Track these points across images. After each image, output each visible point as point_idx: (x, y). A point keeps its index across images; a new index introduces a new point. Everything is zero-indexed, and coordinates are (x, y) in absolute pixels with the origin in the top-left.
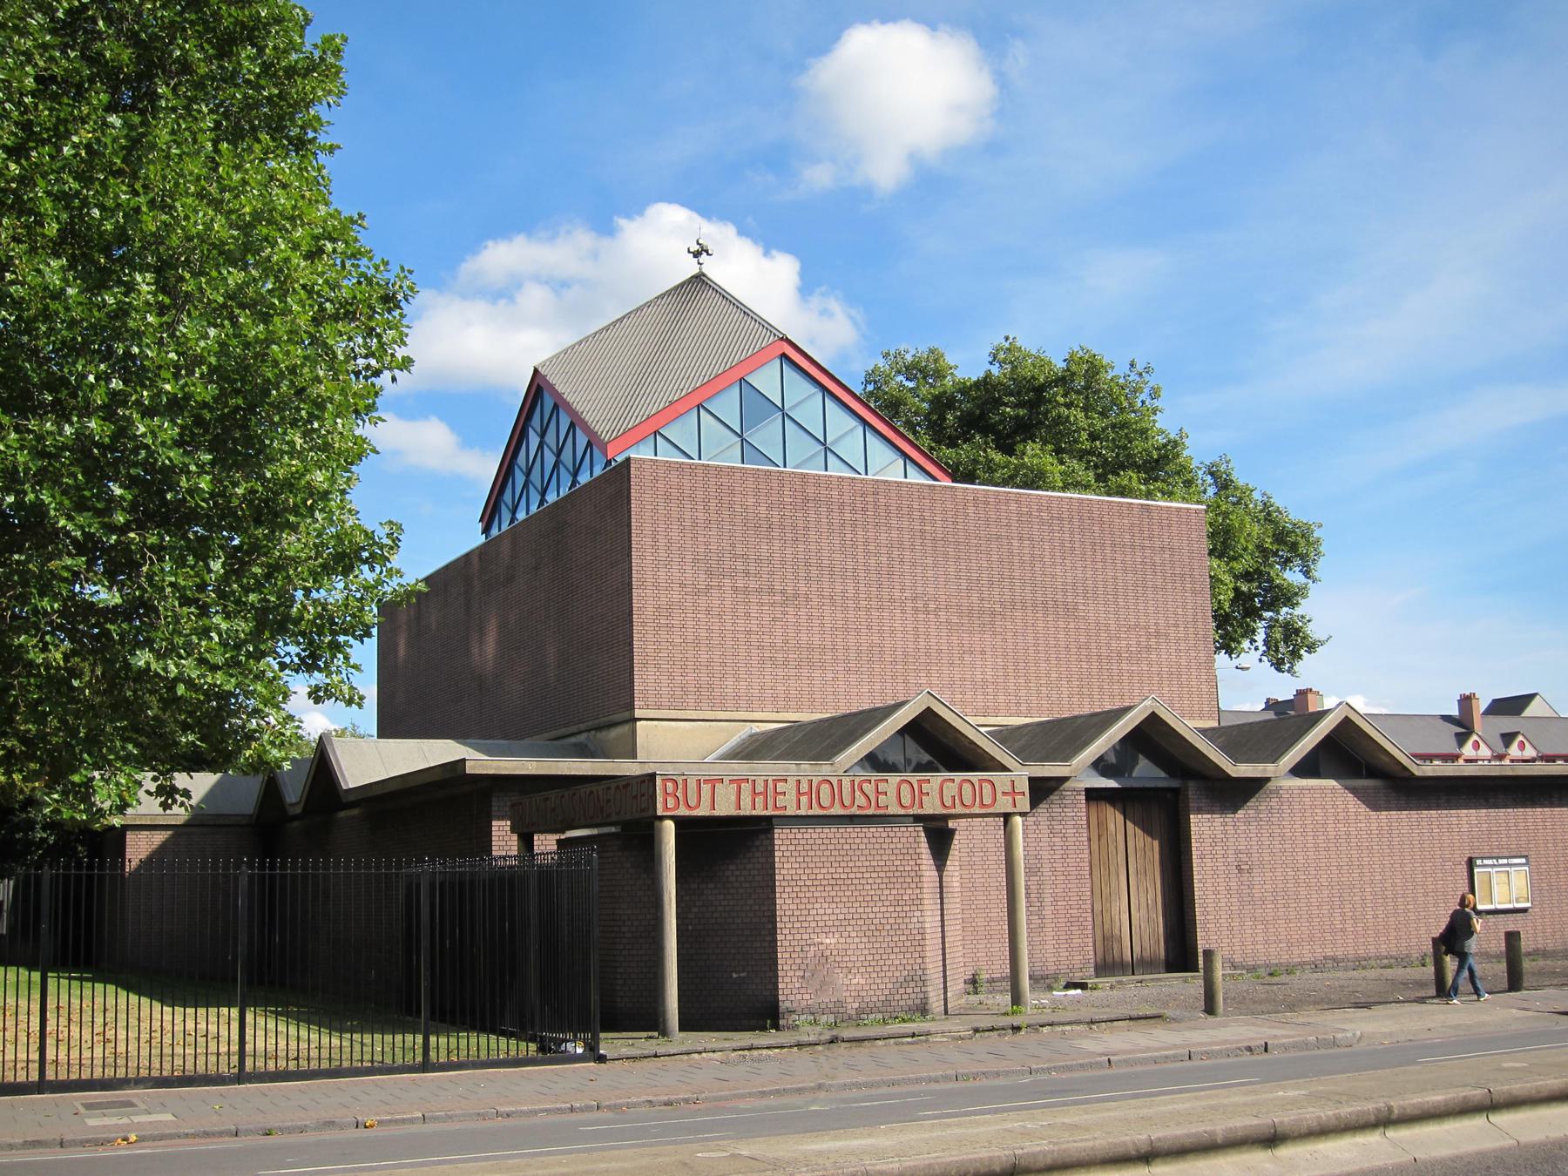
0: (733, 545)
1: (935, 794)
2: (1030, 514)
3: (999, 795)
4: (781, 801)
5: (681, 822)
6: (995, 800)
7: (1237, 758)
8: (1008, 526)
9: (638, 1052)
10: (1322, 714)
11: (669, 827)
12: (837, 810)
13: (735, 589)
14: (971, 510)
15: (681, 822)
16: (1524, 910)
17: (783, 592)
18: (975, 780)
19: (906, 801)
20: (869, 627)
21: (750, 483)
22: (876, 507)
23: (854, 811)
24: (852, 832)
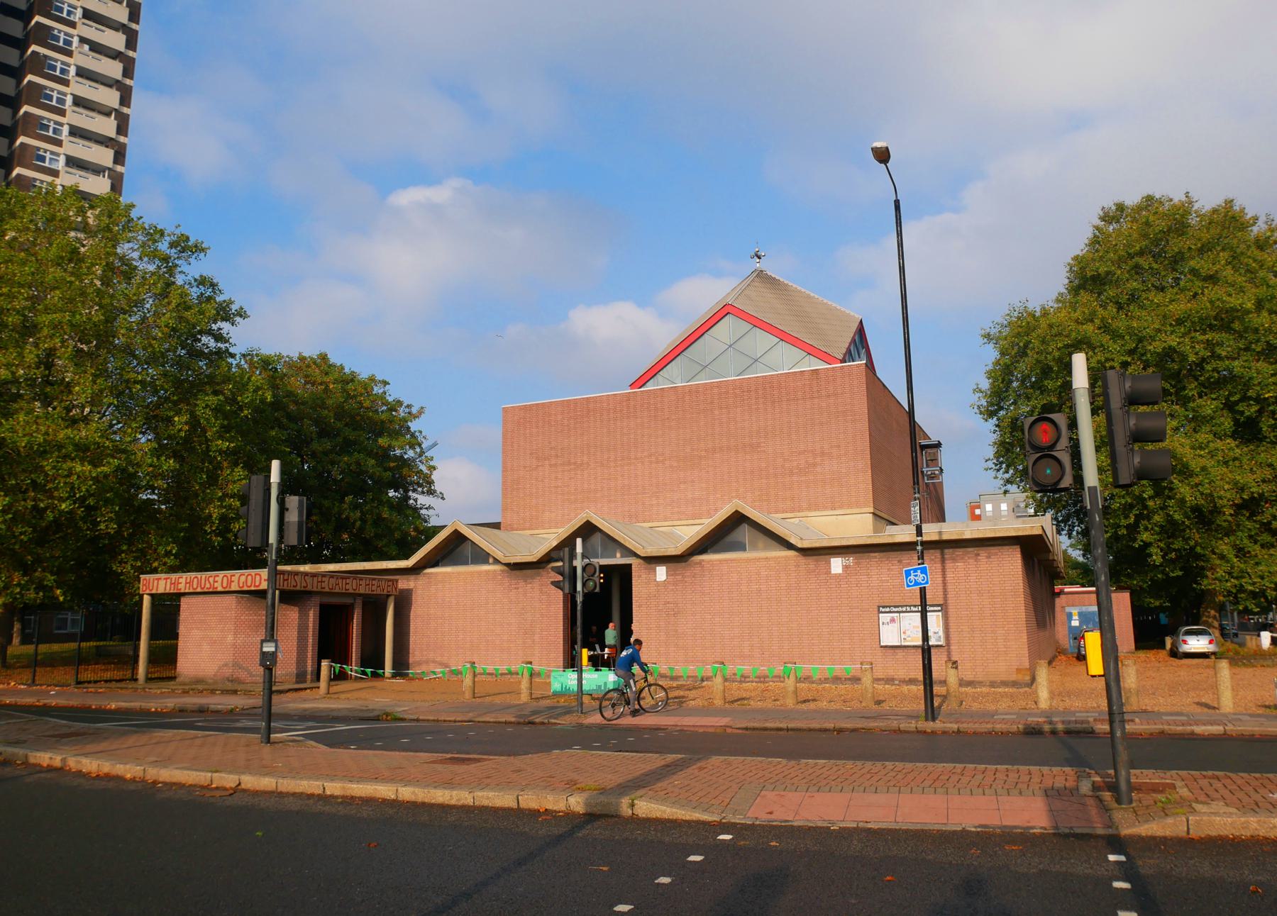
0: (550, 443)
1: (236, 581)
2: (727, 393)
3: (263, 581)
4: (180, 586)
5: (152, 595)
6: (260, 583)
7: (407, 557)
8: (712, 403)
9: (500, 696)
10: (437, 530)
11: (147, 599)
12: (199, 590)
13: (551, 465)
14: (687, 398)
15: (152, 595)
16: (941, 646)
17: (575, 463)
18: (253, 574)
19: (225, 585)
20: (623, 476)
21: (839, 374)
22: (628, 407)
23: (205, 590)
24: (207, 598)
